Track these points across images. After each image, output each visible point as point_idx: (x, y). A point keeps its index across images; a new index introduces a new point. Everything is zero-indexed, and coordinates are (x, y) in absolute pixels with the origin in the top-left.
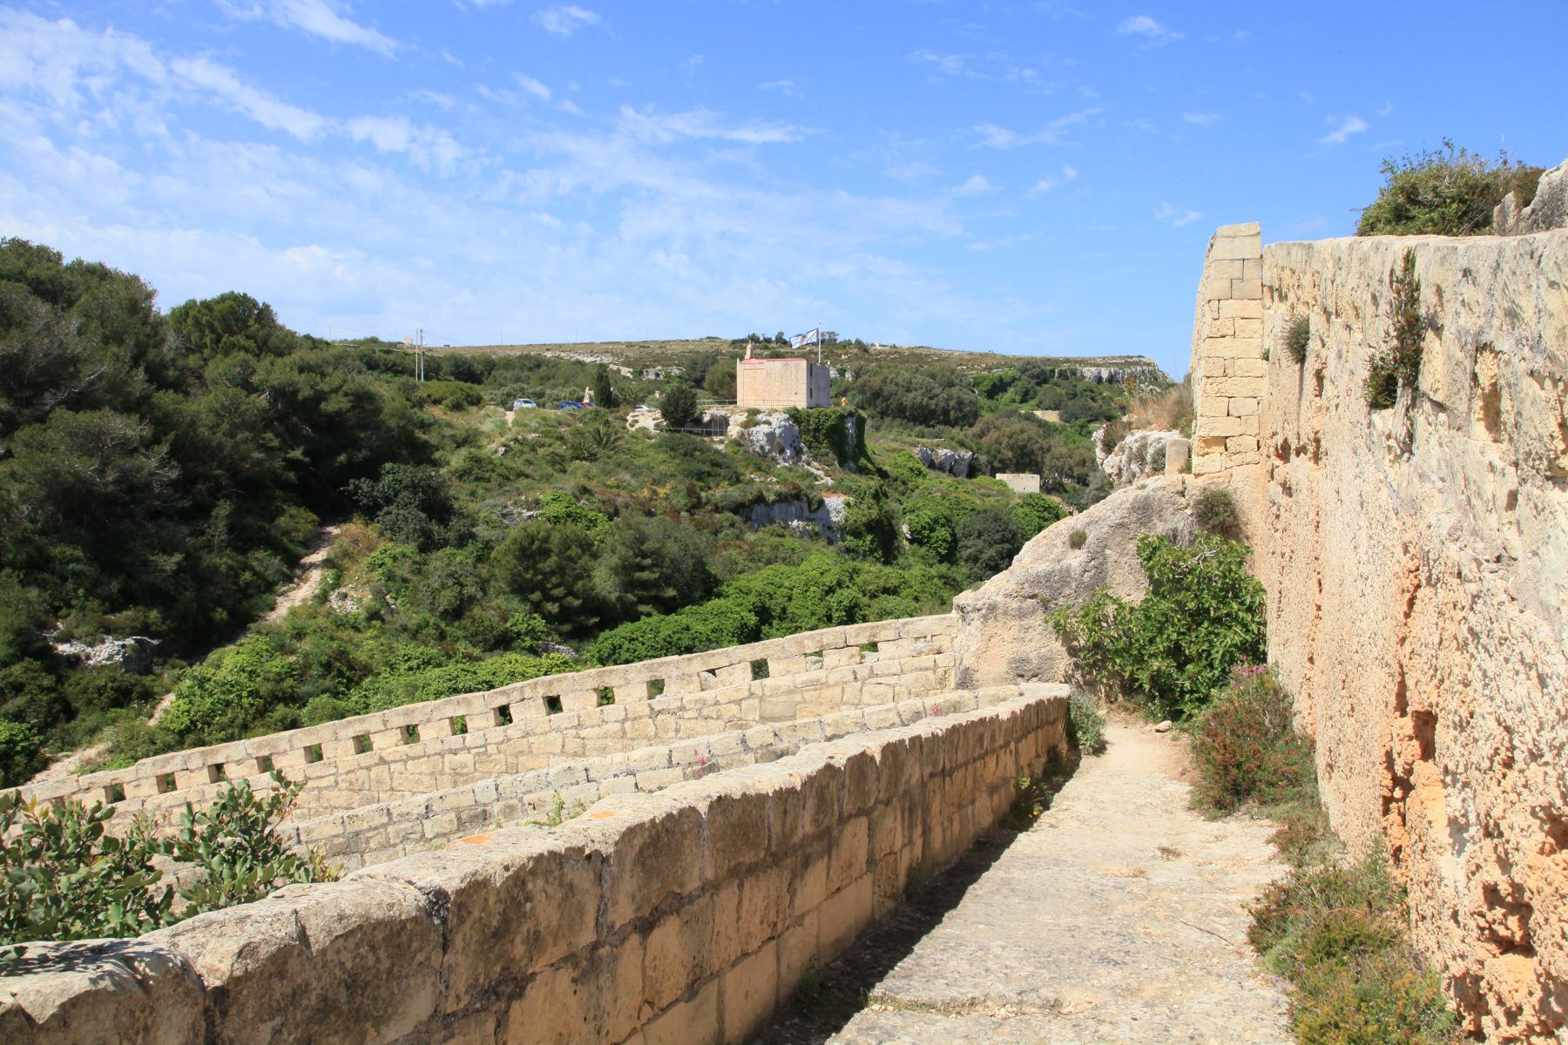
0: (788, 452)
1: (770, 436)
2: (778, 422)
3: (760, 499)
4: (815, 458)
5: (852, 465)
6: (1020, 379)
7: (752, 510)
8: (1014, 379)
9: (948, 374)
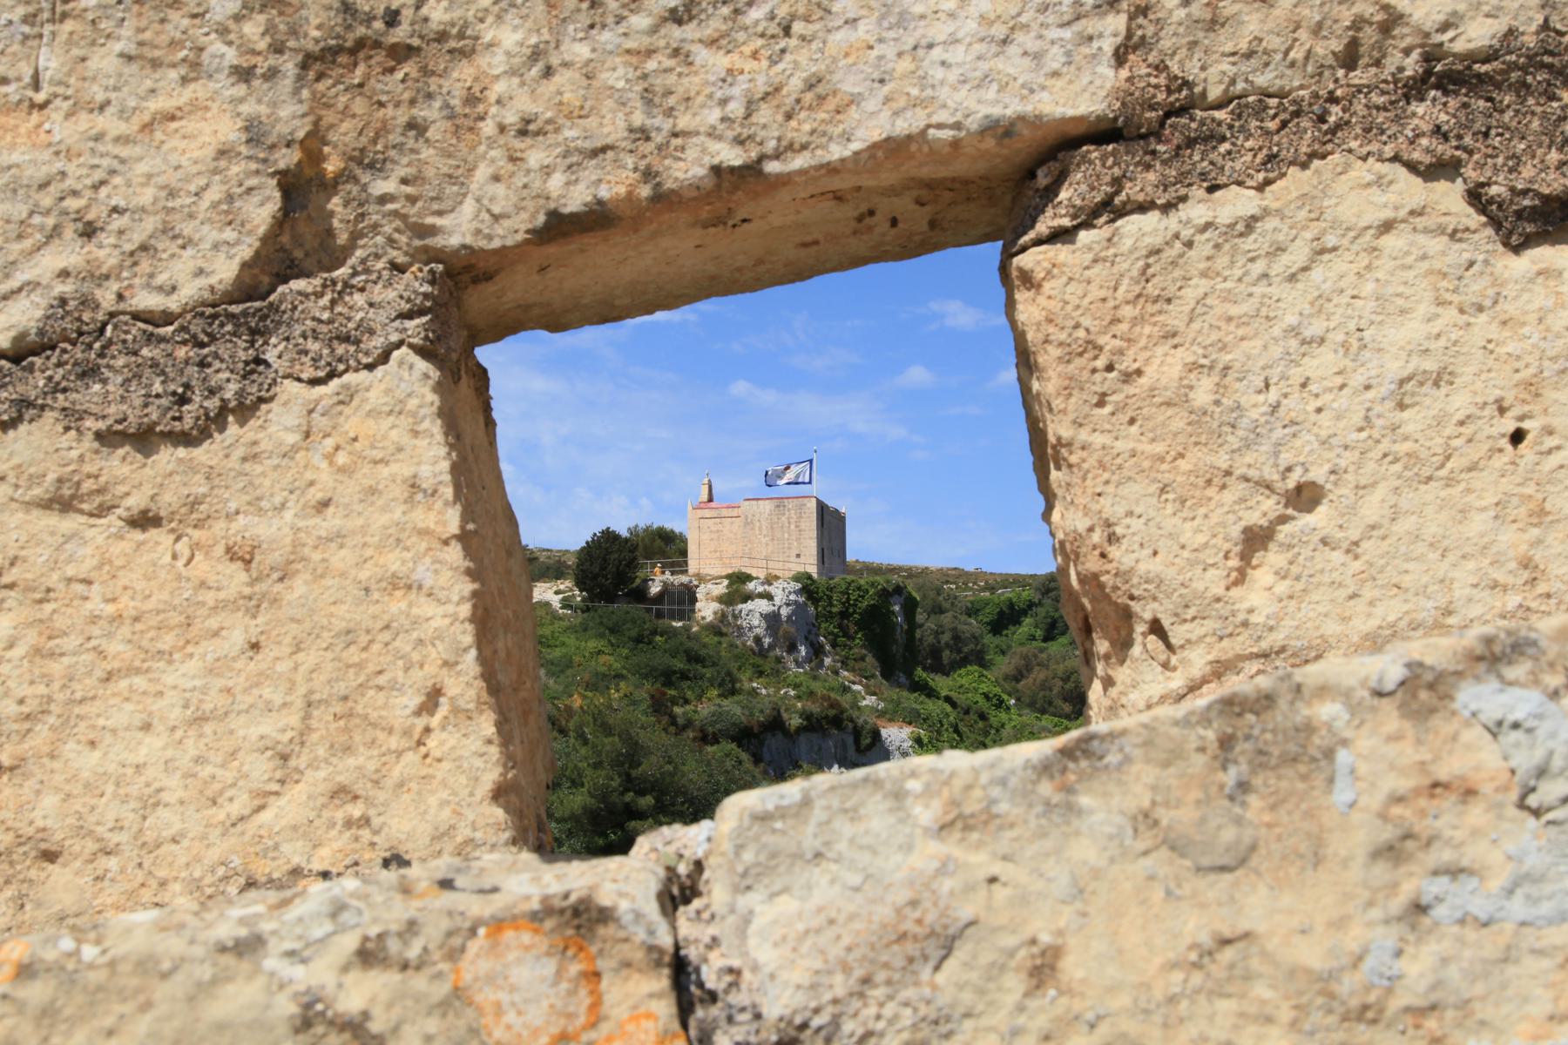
0: (803, 650)
1: (772, 619)
2: (783, 593)
3: (776, 724)
4: (844, 664)
5: (903, 679)
6: (1040, 604)
7: (762, 744)
8: (1031, 605)
9: (932, 594)
